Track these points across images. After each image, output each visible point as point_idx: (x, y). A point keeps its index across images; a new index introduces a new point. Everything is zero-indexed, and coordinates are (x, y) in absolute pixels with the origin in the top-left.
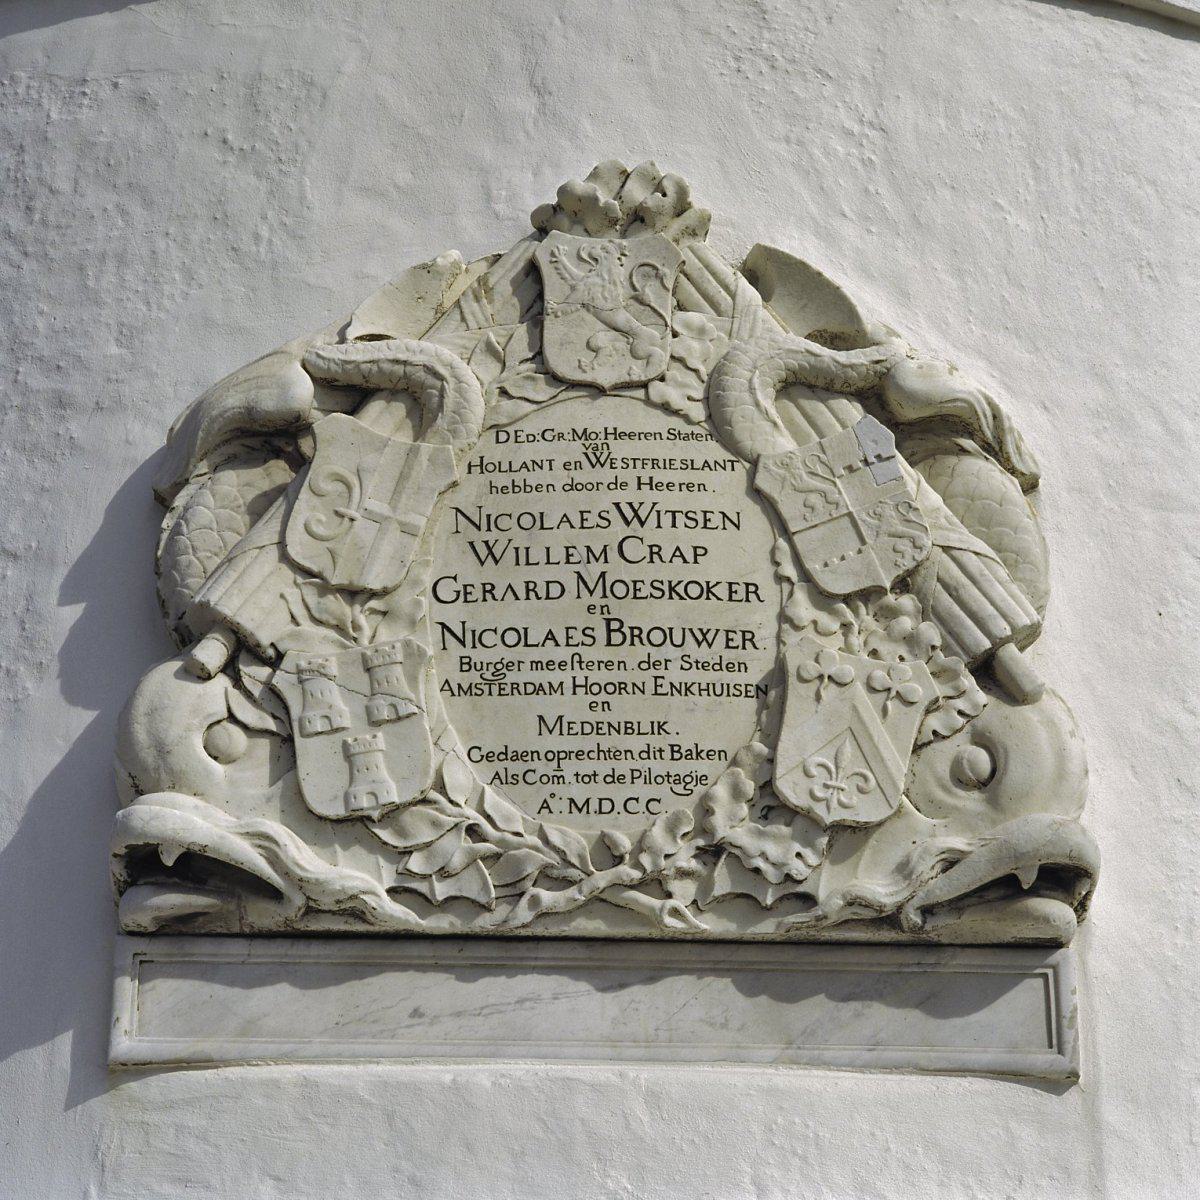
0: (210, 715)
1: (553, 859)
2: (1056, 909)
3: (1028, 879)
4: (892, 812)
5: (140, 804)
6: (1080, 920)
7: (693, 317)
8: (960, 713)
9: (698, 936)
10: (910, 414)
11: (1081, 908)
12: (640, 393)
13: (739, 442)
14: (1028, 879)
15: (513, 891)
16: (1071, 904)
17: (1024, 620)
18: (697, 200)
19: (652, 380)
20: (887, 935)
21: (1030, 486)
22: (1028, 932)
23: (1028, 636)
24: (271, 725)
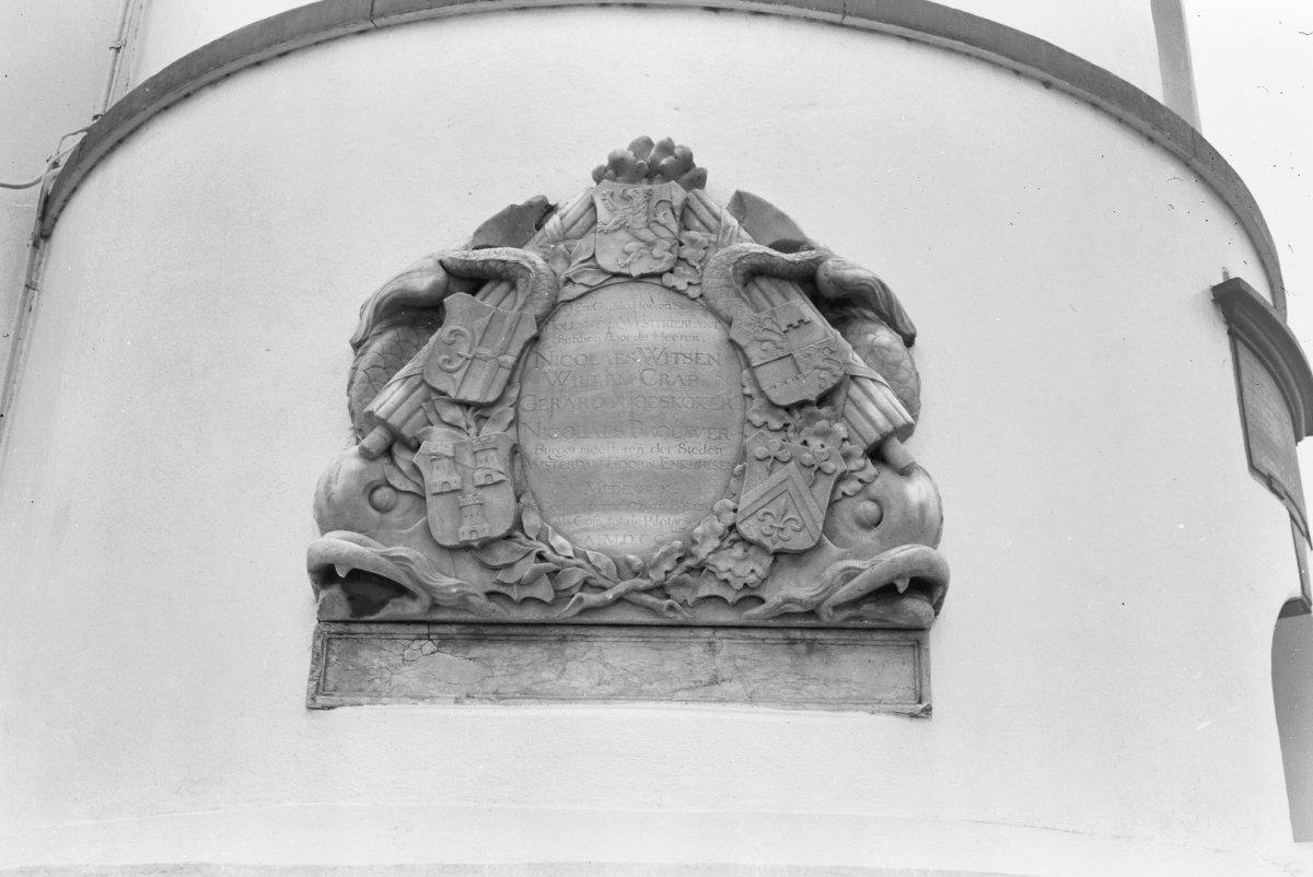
0: (452, 436)
1: (592, 573)
2: (917, 606)
3: (902, 586)
4: (814, 544)
5: (780, 291)
6: (937, 614)
7: (692, 234)
8: (860, 481)
9: (776, 281)
10: (830, 292)
11: (937, 607)
12: (656, 281)
13: (352, 428)
14: (902, 586)
15: (561, 596)
16: (931, 603)
17: (901, 422)
18: (699, 162)
19: (665, 272)
20: (813, 622)
21: (909, 341)
22: (902, 621)
23: (905, 432)
24: (411, 488)
